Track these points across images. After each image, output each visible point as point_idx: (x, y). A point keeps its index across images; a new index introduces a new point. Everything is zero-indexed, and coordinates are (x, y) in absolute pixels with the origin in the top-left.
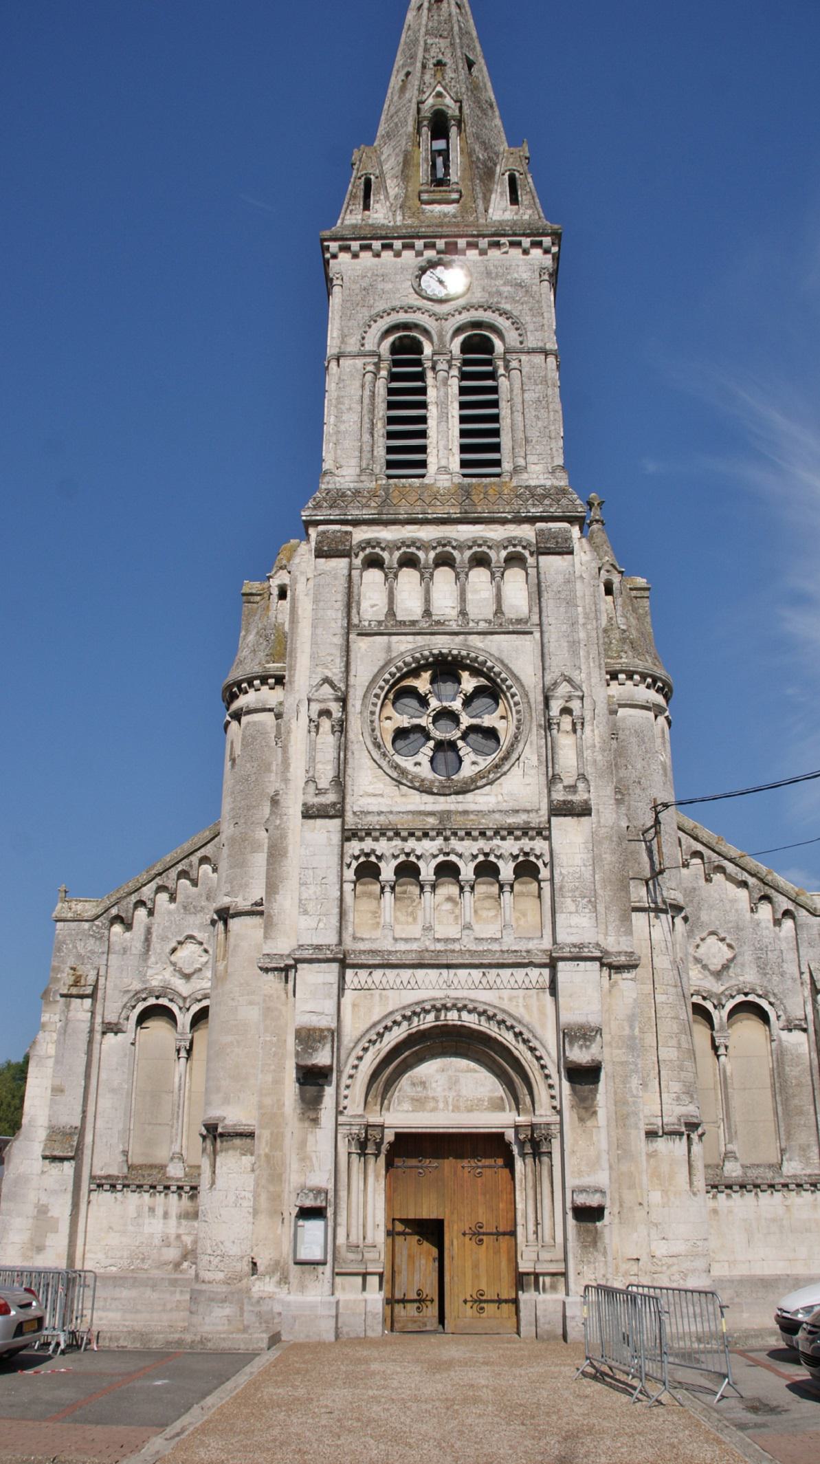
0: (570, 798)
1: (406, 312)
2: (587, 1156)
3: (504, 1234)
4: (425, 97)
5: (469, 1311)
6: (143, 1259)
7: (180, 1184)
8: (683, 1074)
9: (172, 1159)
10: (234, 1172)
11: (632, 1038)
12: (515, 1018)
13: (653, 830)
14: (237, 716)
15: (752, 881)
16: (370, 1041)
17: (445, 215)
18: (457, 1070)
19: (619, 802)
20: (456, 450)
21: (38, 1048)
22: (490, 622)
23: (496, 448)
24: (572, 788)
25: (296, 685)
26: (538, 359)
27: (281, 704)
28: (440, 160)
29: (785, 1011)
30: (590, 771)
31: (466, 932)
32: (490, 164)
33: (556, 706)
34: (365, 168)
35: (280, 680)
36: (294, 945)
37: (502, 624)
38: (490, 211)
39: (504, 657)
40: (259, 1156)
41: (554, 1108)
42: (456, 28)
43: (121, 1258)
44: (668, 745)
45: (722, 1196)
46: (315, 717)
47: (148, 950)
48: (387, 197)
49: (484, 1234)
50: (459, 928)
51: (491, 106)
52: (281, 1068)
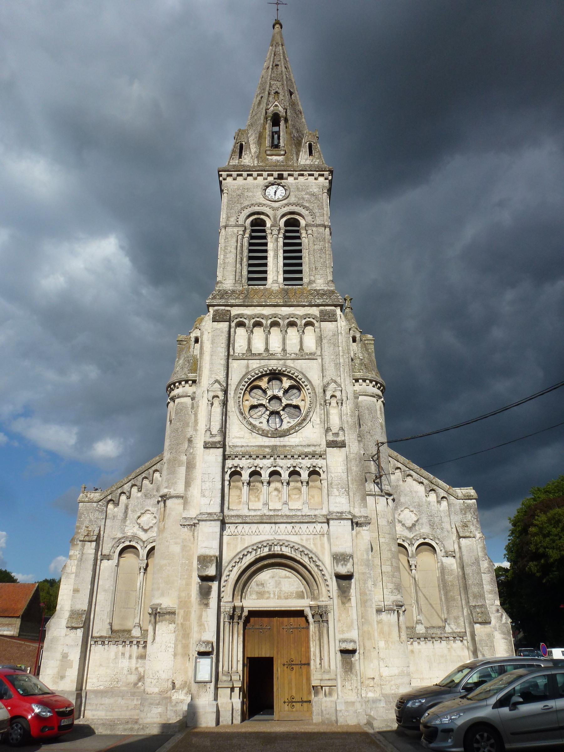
0: (335, 439)
1: (259, 206)
2: (344, 625)
3: (305, 664)
4: (269, 107)
5: (286, 707)
6: (118, 682)
7: (138, 640)
8: (394, 579)
9: (135, 627)
10: (165, 633)
11: (368, 560)
12: (309, 550)
13: (376, 456)
14: (173, 399)
15: (425, 482)
16: (236, 562)
17: (278, 161)
18: (280, 577)
19: (359, 441)
20: (281, 272)
21: (67, 569)
22: (297, 354)
23: (300, 272)
24: (337, 434)
25: (202, 384)
26: (321, 229)
27: (194, 393)
28: (276, 136)
29: (444, 547)
30: (345, 426)
31: (285, 506)
32: (300, 139)
33: (328, 397)
34: (240, 139)
35: (194, 382)
36: (198, 512)
37: (302, 355)
38: (299, 160)
39: (303, 371)
40: (178, 624)
41: (329, 597)
42: (285, 77)
43: (106, 681)
44: (383, 415)
45: (415, 644)
46: (211, 399)
47: (126, 517)
48: (250, 152)
49: (294, 665)
50: (281, 504)
51: (301, 113)
52: (190, 577)
